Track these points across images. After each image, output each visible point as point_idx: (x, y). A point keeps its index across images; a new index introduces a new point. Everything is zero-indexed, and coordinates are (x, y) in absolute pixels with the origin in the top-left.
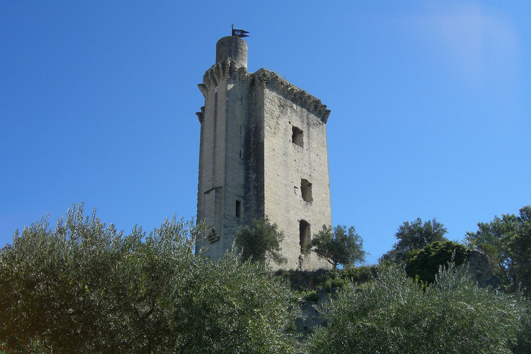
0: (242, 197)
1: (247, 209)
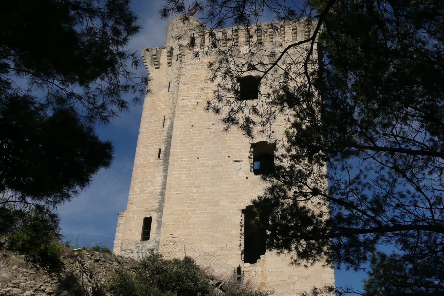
0: (155, 210)
1: (160, 225)
